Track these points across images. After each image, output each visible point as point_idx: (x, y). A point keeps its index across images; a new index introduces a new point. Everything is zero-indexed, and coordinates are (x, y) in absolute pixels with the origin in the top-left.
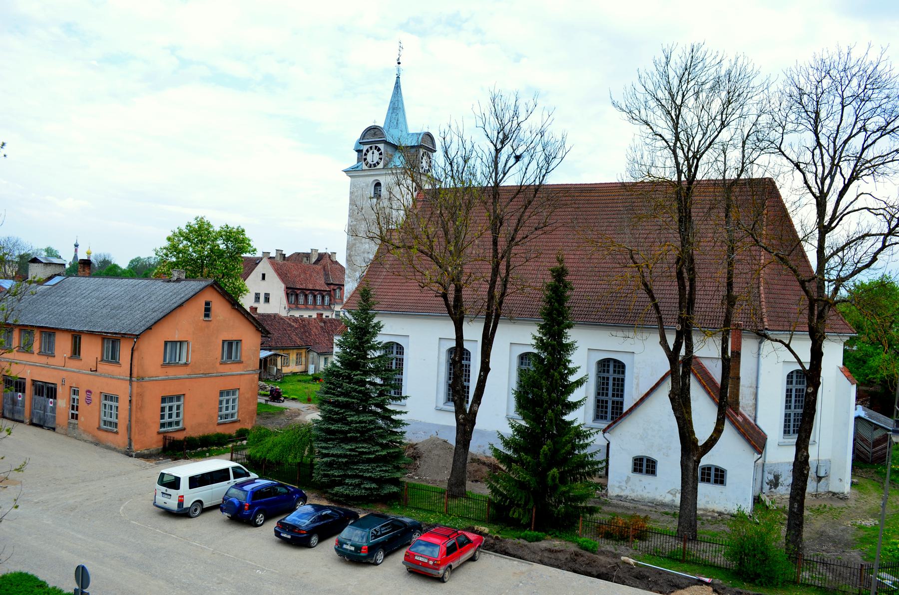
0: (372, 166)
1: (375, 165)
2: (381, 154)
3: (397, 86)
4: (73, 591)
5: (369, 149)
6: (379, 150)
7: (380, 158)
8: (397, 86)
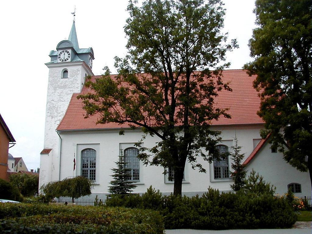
0: (64, 60)
1: (65, 60)
2: (69, 54)
3: (74, 25)
4: (252, 76)
5: (62, 52)
6: (68, 52)
7: (60, 55)
8: (74, 25)
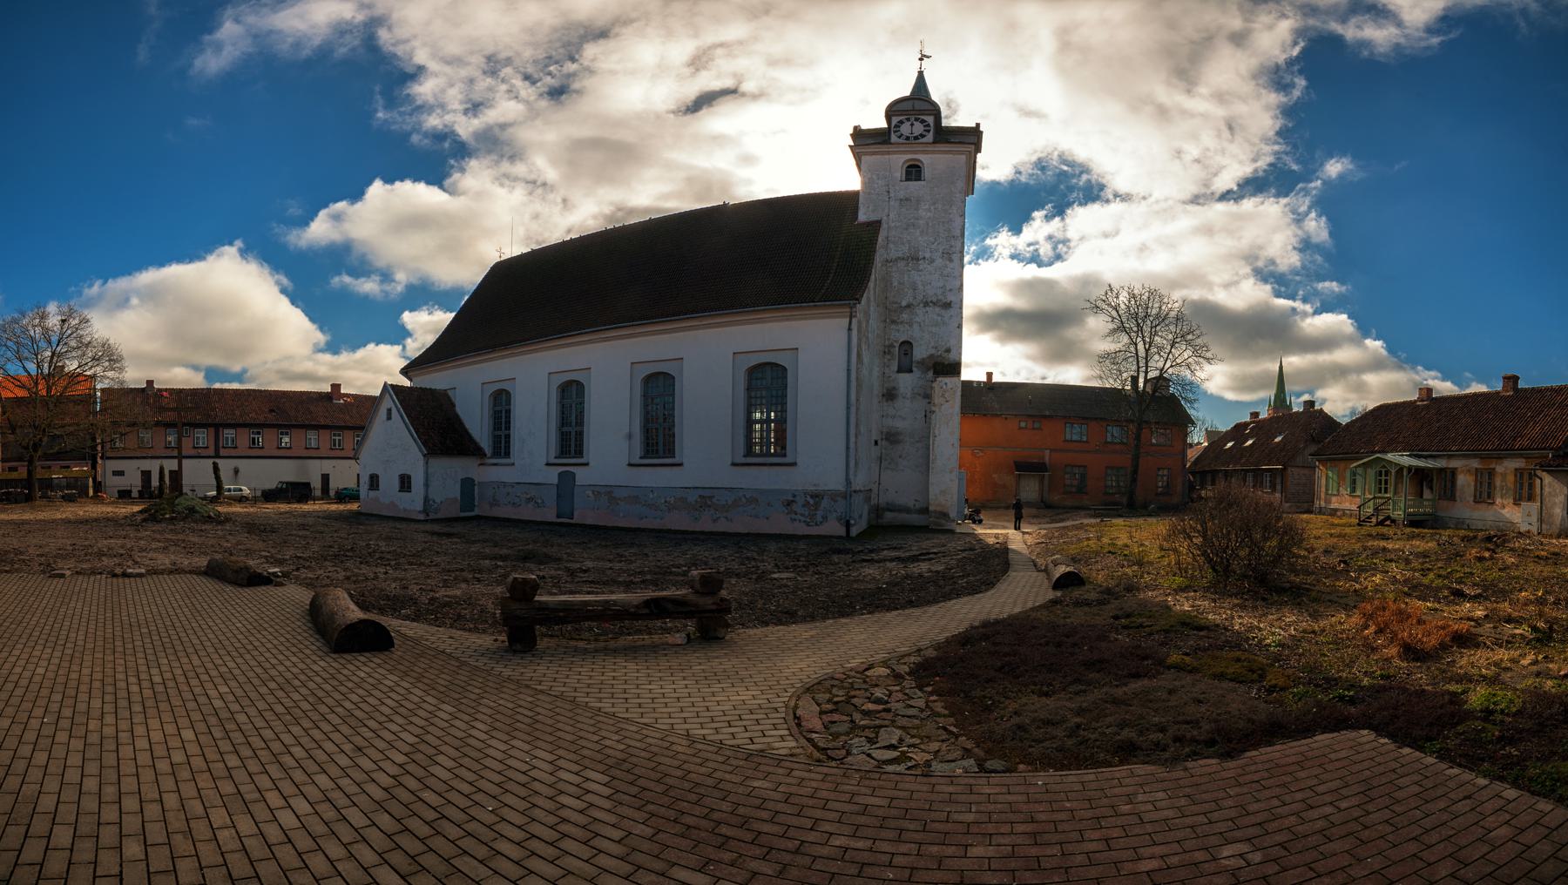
1: (916, 138)
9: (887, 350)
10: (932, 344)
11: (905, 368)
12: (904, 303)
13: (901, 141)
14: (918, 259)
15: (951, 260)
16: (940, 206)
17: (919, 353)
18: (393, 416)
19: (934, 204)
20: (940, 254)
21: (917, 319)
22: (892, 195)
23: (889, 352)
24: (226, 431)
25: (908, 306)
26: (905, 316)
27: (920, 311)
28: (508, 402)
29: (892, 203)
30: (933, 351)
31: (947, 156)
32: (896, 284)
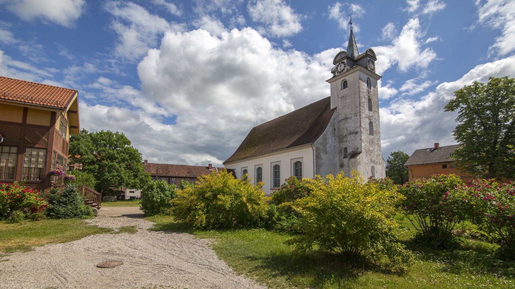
1: (342, 71)
9: (340, 152)
10: (353, 147)
11: (345, 157)
12: (344, 135)
13: (338, 74)
14: (347, 119)
15: (357, 116)
16: (352, 96)
17: (349, 151)
18: (130, 193)
19: (350, 96)
20: (353, 115)
21: (348, 140)
22: (339, 96)
23: (341, 152)
24: (172, 179)
25: (345, 136)
26: (345, 139)
27: (349, 137)
28: (301, 166)
29: (339, 100)
30: (353, 150)
31: (353, 74)
32: (342, 129)
